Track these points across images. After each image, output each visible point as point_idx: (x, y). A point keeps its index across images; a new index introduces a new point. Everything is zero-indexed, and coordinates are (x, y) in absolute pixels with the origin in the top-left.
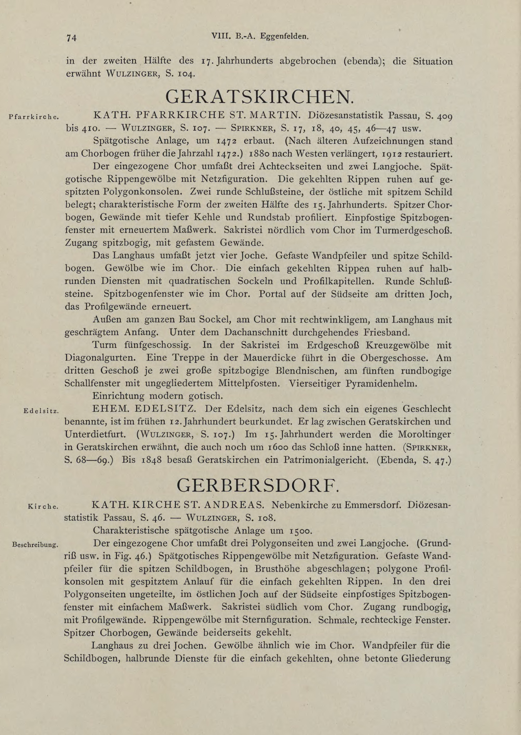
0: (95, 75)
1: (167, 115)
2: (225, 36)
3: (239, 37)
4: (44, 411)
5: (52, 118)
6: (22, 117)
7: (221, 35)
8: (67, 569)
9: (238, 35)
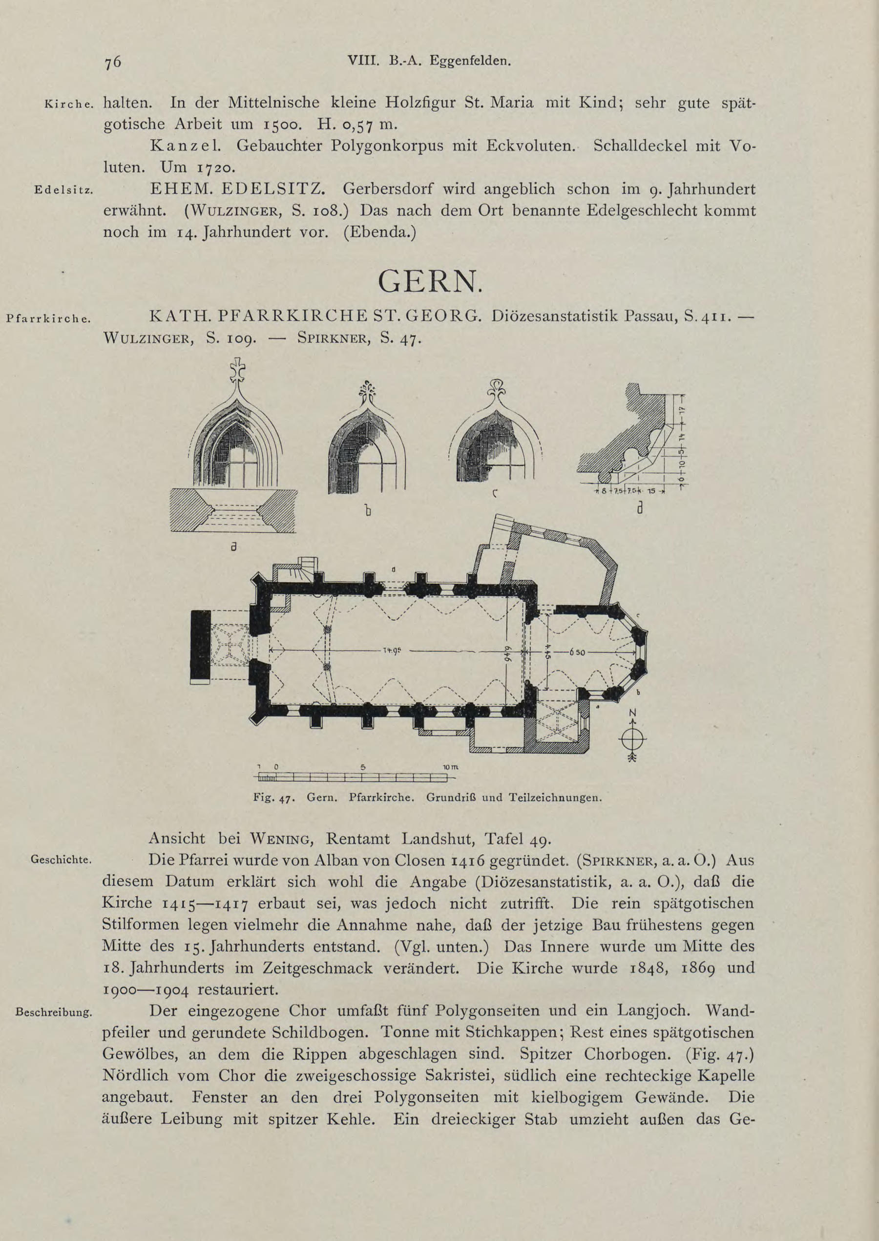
0: (152, 213)
1: (270, 315)
2: (370, 62)
3: (395, 62)
4: (69, 191)
5: (80, 320)
6: (29, 320)
7: (364, 59)
8: (107, 1034)
9: (394, 60)
